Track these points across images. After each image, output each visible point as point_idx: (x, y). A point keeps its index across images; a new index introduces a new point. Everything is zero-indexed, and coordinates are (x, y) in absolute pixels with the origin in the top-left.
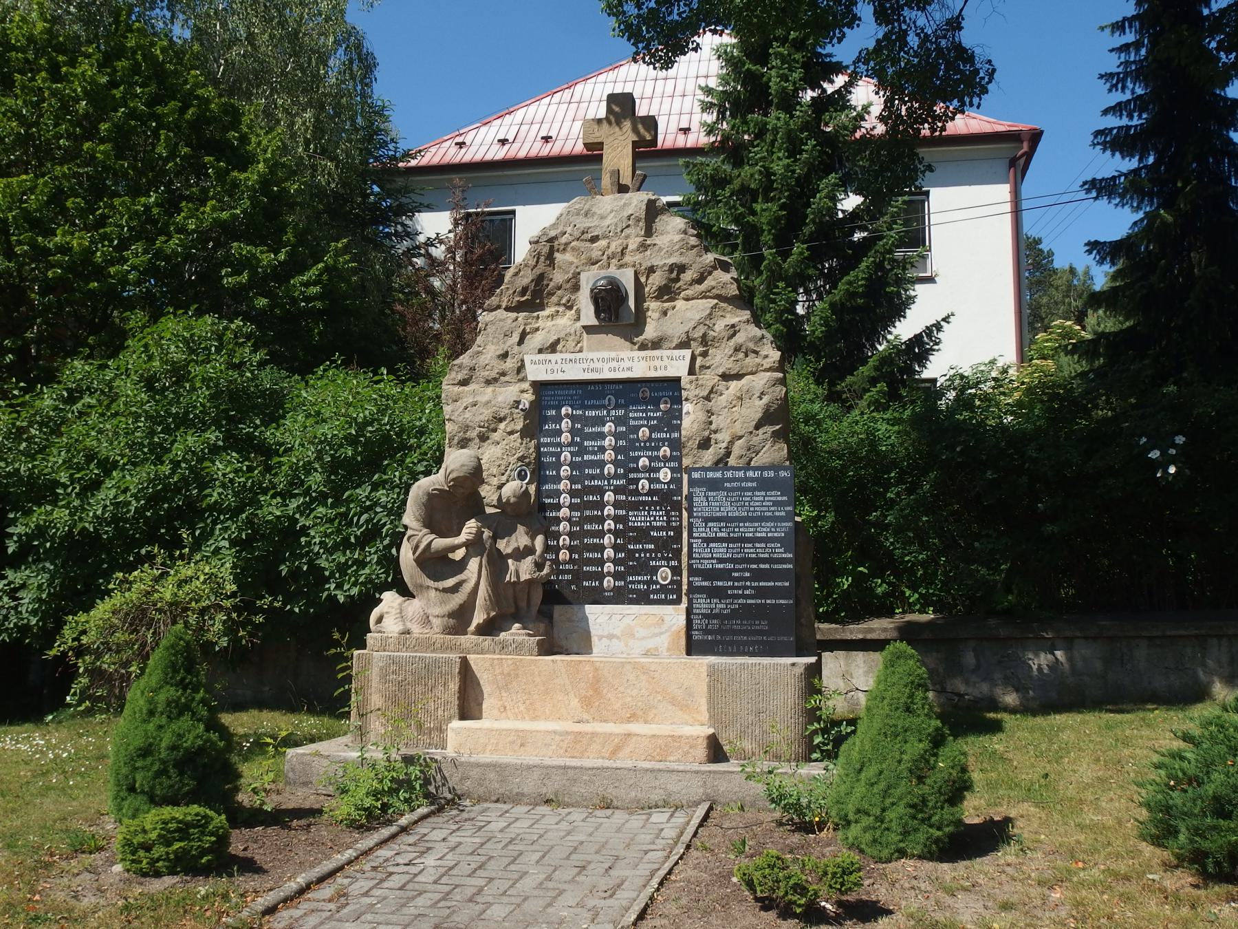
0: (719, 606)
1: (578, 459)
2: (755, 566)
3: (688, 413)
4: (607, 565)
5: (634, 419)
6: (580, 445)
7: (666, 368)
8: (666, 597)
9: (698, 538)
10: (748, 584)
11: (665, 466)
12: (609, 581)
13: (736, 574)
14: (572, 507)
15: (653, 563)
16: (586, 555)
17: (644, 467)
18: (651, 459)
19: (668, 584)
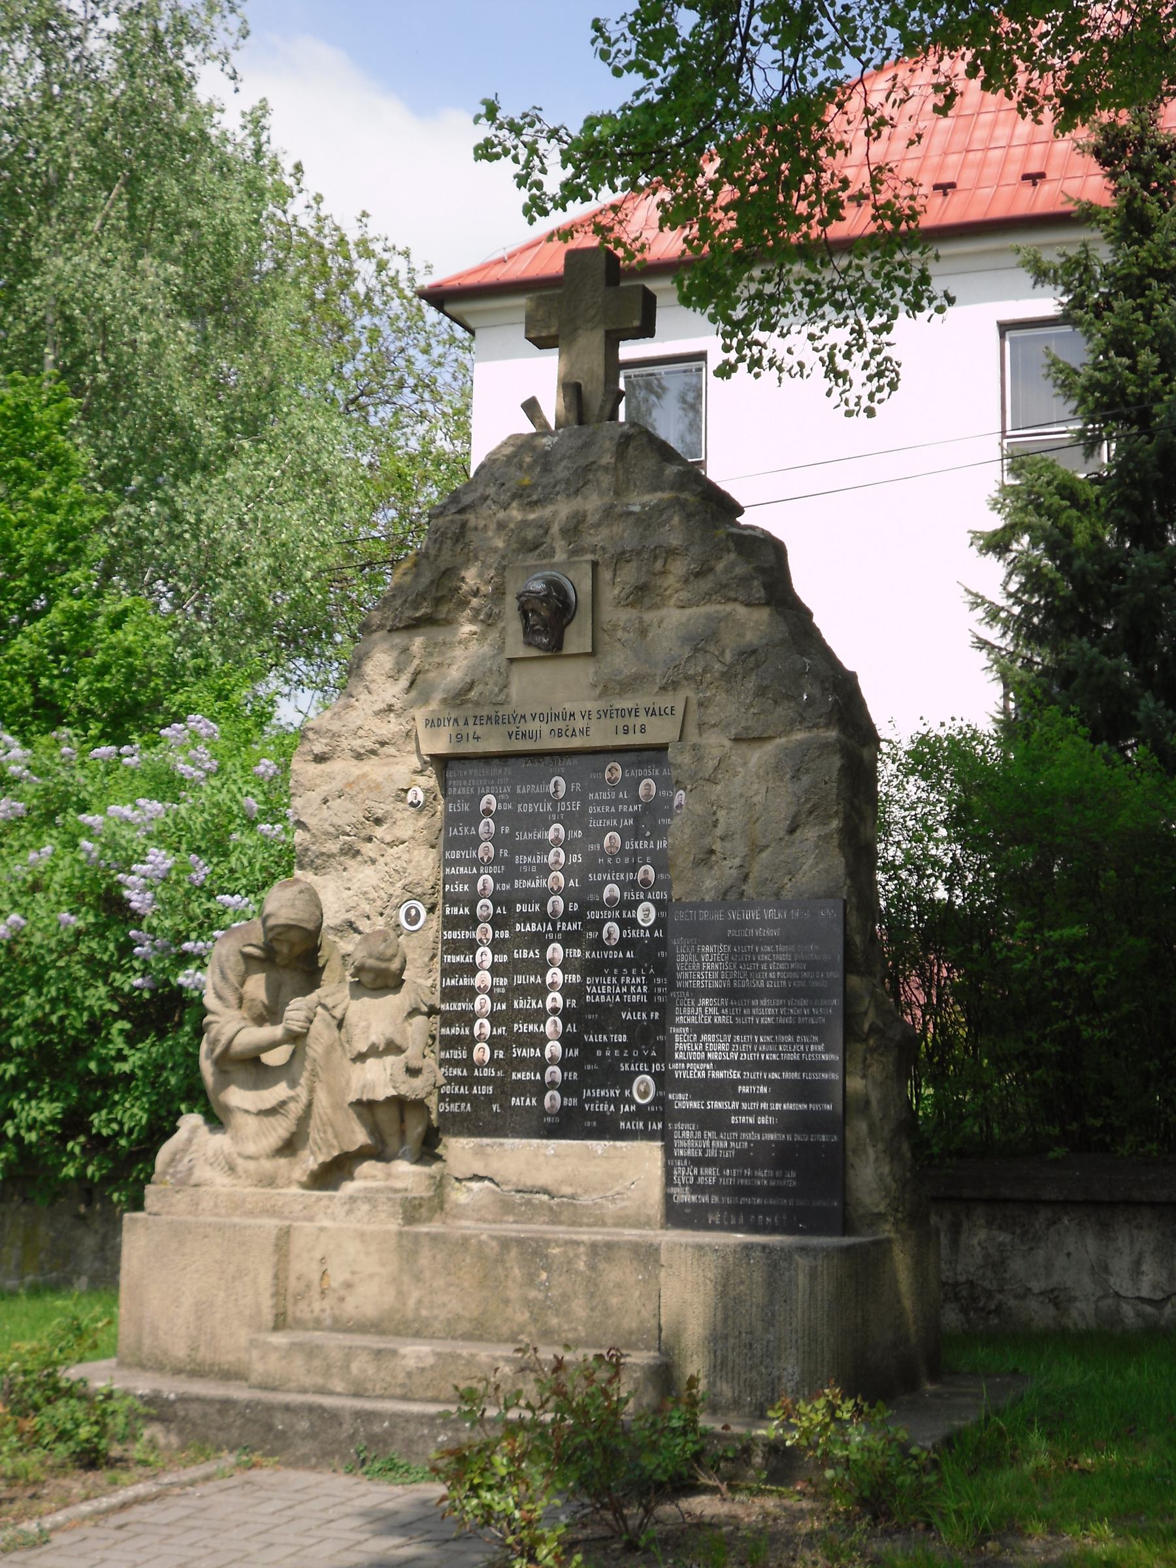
0: (717, 1144)
1: (505, 887)
2: (775, 1076)
3: (680, 806)
4: (550, 1069)
5: (597, 816)
6: (509, 862)
7: (643, 729)
8: (645, 1126)
9: (684, 1025)
10: (764, 1105)
11: (646, 900)
12: (552, 1098)
13: (745, 1089)
14: (495, 970)
15: (624, 1067)
16: (517, 1052)
17: (611, 900)
18: (622, 886)
19: (650, 1104)
